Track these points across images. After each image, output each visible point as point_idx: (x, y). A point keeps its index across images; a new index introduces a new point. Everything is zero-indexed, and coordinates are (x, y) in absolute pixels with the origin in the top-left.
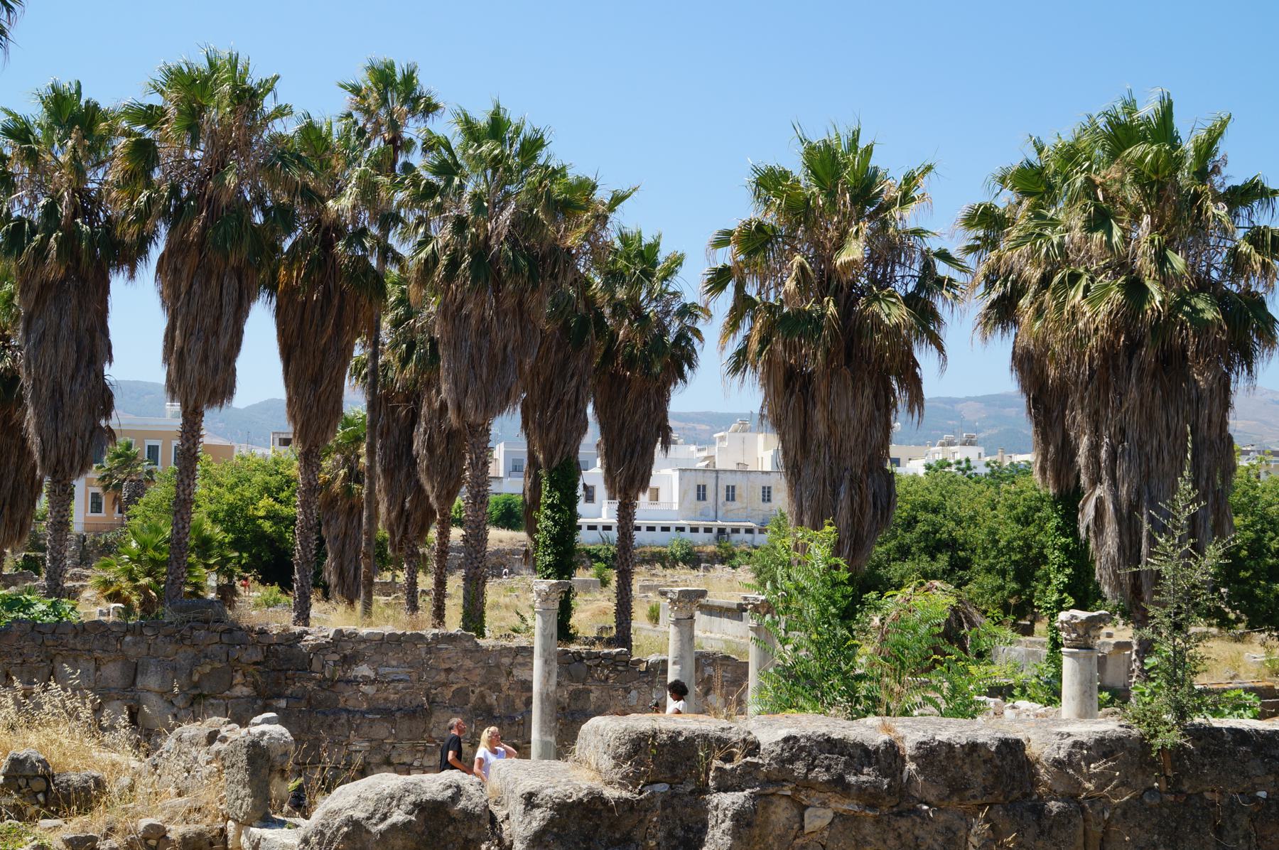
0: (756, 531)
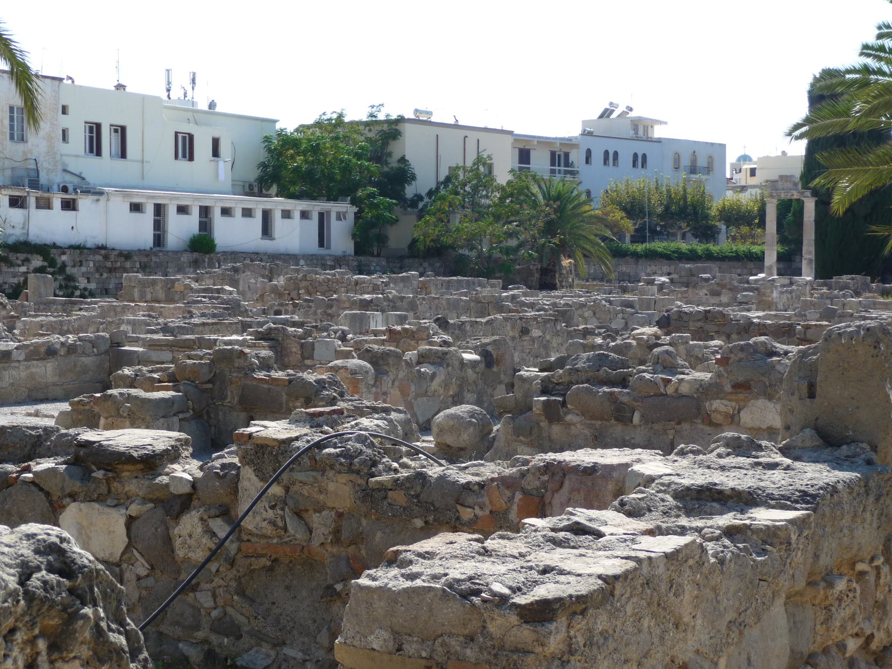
0: (32, 201)
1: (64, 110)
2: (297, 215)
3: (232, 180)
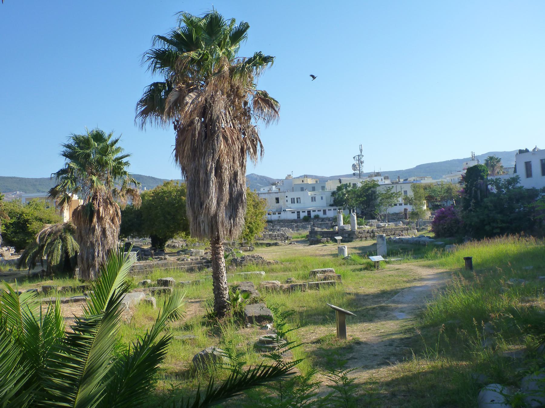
1: (287, 197)
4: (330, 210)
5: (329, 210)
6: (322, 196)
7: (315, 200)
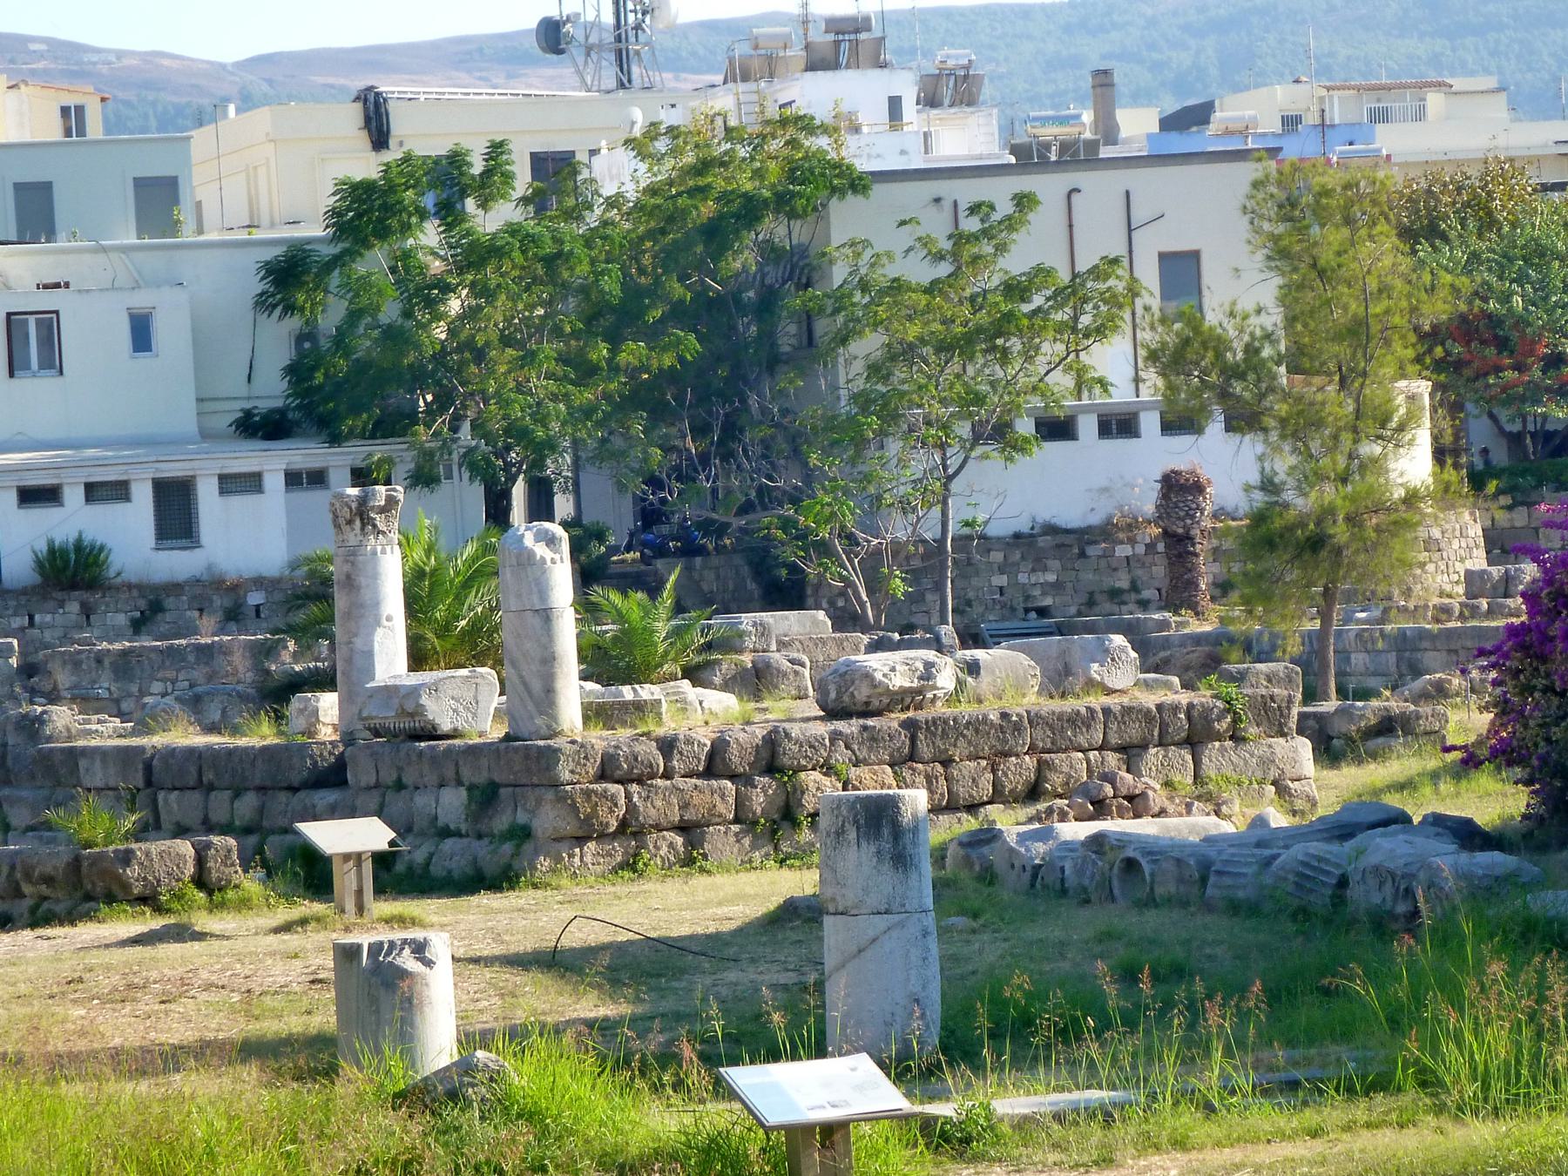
2: (274, 482)
3: (200, 400)
4: (251, 483)
5: (232, 484)
6: (141, 300)
7: (52, 361)
